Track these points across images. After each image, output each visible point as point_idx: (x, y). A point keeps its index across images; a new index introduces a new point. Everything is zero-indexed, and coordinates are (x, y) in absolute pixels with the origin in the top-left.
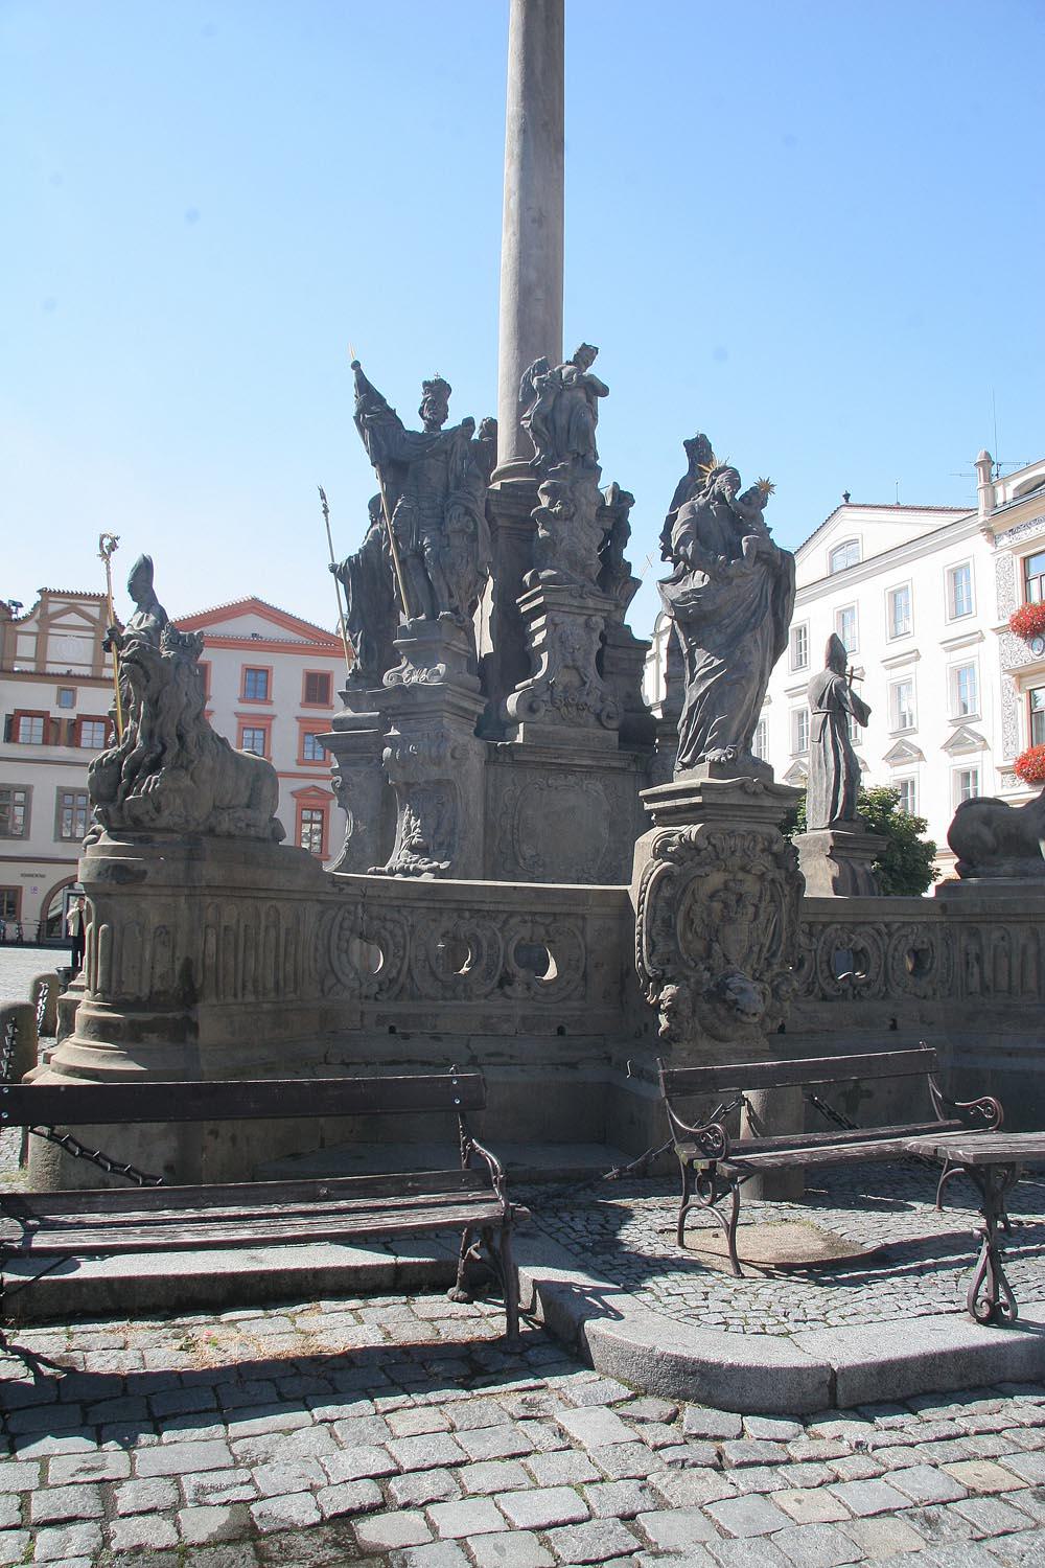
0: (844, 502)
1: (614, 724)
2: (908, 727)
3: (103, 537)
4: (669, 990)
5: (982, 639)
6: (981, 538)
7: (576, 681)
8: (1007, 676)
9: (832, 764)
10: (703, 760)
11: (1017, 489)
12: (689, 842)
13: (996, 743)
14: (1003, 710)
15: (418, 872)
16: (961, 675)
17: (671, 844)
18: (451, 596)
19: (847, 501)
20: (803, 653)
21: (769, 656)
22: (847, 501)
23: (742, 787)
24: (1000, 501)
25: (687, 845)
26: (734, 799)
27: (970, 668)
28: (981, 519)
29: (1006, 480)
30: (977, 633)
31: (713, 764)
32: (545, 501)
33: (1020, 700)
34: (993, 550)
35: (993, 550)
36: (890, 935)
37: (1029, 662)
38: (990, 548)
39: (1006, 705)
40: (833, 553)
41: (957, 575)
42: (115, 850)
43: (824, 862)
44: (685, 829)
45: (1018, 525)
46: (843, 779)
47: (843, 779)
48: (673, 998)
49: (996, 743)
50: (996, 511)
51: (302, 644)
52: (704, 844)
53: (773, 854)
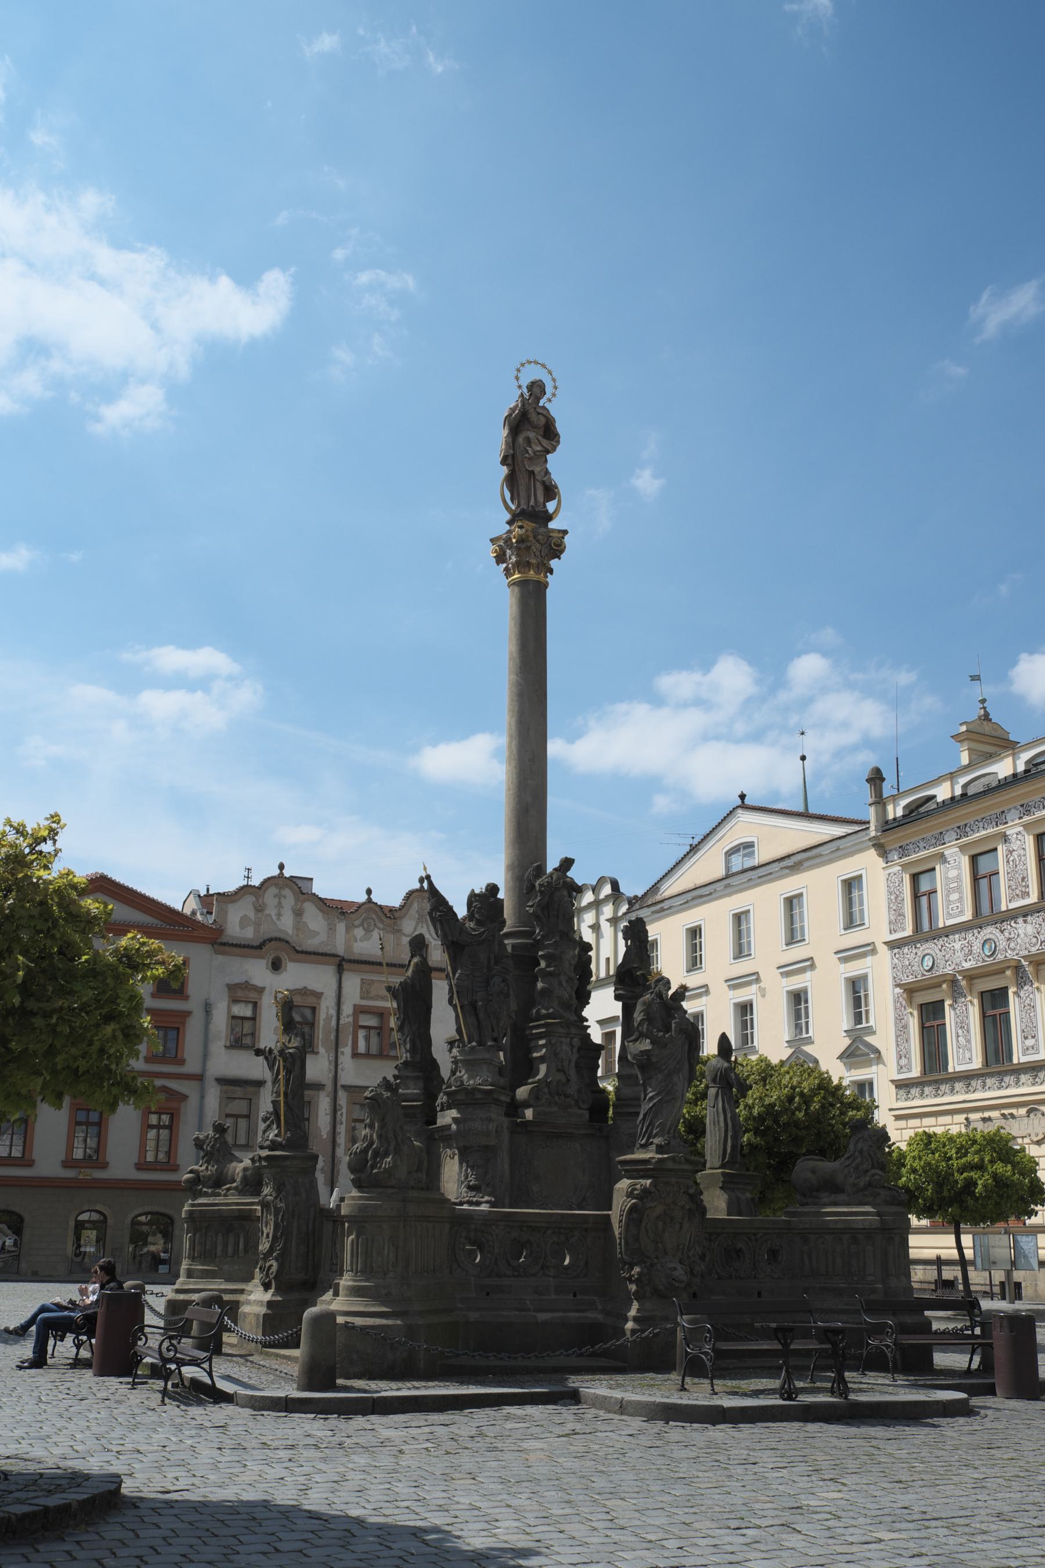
0: (739, 802)
1: (586, 1106)
2: (804, 1036)
3: (277, 992)
4: (637, 1269)
5: (874, 951)
6: (872, 853)
7: (564, 1079)
8: (898, 990)
9: (722, 1124)
10: (652, 1143)
11: (904, 808)
12: (645, 1188)
13: (889, 1054)
14: (896, 1023)
15: (478, 1204)
16: (857, 991)
17: (635, 1189)
18: (493, 1031)
19: (743, 802)
20: (698, 954)
21: (686, 1085)
22: (743, 802)
23: (673, 1159)
24: (891, 816)
25: (645, 1191)
26: (670, 1165)
27: (864, 978)
28: (873, 833)
29: (894, 798)
30: (868, 945)
31: (658, 1146)
32: (543, 964)
33: (911, 1013)
34: (885, 865)
35: (885, 865)
36: (756, 1240)
37: (920, 978)
38: (880, 862)
39: (899, 1019)
40: (729, 854)
41: (851, 885)
42: (361, 1198)
43: (719, 1192)
44: (643, 1181)
45: (908, 842)
46: (730, 1134)
47: (730, 1134)
48: (639, 1274)
49: (889, 1054)
50: (888, 826)
51: (160, 928)
52: (653, 1190)
53: (689, 1194)
